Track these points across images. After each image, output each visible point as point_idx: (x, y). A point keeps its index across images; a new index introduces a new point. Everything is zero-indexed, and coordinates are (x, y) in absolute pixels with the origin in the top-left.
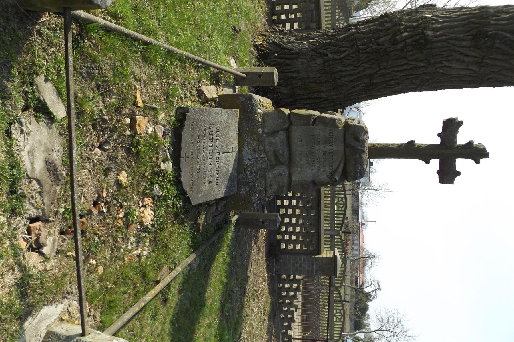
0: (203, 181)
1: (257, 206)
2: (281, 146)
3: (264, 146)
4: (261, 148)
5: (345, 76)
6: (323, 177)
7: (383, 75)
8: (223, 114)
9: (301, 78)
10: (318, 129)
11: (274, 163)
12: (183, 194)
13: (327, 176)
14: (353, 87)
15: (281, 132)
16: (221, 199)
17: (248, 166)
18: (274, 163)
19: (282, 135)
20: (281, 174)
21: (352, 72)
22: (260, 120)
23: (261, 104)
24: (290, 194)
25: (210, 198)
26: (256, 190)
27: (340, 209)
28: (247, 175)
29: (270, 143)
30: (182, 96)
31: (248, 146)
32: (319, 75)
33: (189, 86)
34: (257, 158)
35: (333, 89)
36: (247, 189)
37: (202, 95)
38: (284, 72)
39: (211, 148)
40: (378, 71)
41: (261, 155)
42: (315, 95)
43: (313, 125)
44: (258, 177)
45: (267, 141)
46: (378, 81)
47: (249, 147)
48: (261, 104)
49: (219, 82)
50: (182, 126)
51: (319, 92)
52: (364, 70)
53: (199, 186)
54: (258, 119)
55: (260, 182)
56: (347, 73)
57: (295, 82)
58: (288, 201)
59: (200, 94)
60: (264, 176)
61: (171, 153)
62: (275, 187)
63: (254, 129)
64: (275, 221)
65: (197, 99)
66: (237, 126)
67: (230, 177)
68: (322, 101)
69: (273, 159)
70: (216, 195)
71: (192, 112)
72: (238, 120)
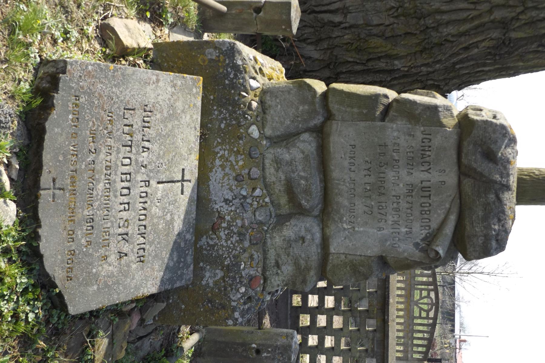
0: (102, 251)
1: (242, 316)
2: (304, 171)
3: (263, 169)
4: (256, 172)
5: (448, 23)
6: (407, 249)
7: (532, 23)
8: (161, 84)
9: (351, 27)
10: (395, 131)
11: (285, 210)
12: (44, 286)
13: (416, 245)
14: (466, 49)
15: (306, 136)
16: (152, 297)
17: (221, 218)
18: (285, 210)
19: (307, 144)
20: (303, 239)
21: (465, 15)
22: (254, 104)
23: (257, 67)
24: (322, 284)
25: (120, 295)
26: (241, 277)
27: (424, 314)
28: (219, 238)
29: (278, 162)
30: (57, 34)
31: (223, 167)
32: (392, 20)
33: (78, 14)
34: (245, 197)
35: (421, 52)
36: (220, 274)
37: (111, 39)
38: (314, 12)
39: (125, 169)
40: (522, 12)
41: (254, 189)
42: (382, 65)
43: (383, 119)
44: (247, 244)
45: (269, 156)
46: (520, 35)
47: (227, 170)
48: (257, 67)
49: (161, 16)
50: (47, 106)
51: (389, 56)
52: (490, 12)
53: (91, 264)
54: (250, 104)
55: (251, 257)
56: (454, 17)
57: (336, 33)
58: (316, 337)
59: (106, 34)
60: (261, 243)
61: (14, 175)
62: (288, 269)
63: (239, 125)
64: (287, 348)
65: (98, 46)
66: (198, 117)
67: (175, 242)
68: (395, 78)
69: (284, 200)
70: (137, 288)
71: (77, 74)
72: (199, 104)
